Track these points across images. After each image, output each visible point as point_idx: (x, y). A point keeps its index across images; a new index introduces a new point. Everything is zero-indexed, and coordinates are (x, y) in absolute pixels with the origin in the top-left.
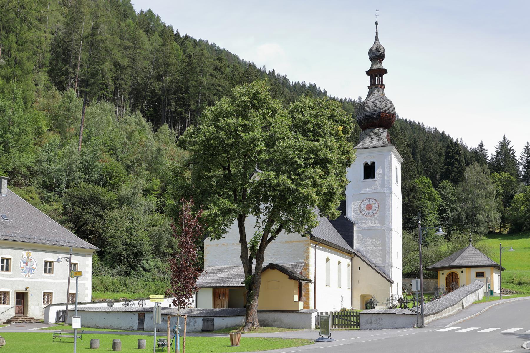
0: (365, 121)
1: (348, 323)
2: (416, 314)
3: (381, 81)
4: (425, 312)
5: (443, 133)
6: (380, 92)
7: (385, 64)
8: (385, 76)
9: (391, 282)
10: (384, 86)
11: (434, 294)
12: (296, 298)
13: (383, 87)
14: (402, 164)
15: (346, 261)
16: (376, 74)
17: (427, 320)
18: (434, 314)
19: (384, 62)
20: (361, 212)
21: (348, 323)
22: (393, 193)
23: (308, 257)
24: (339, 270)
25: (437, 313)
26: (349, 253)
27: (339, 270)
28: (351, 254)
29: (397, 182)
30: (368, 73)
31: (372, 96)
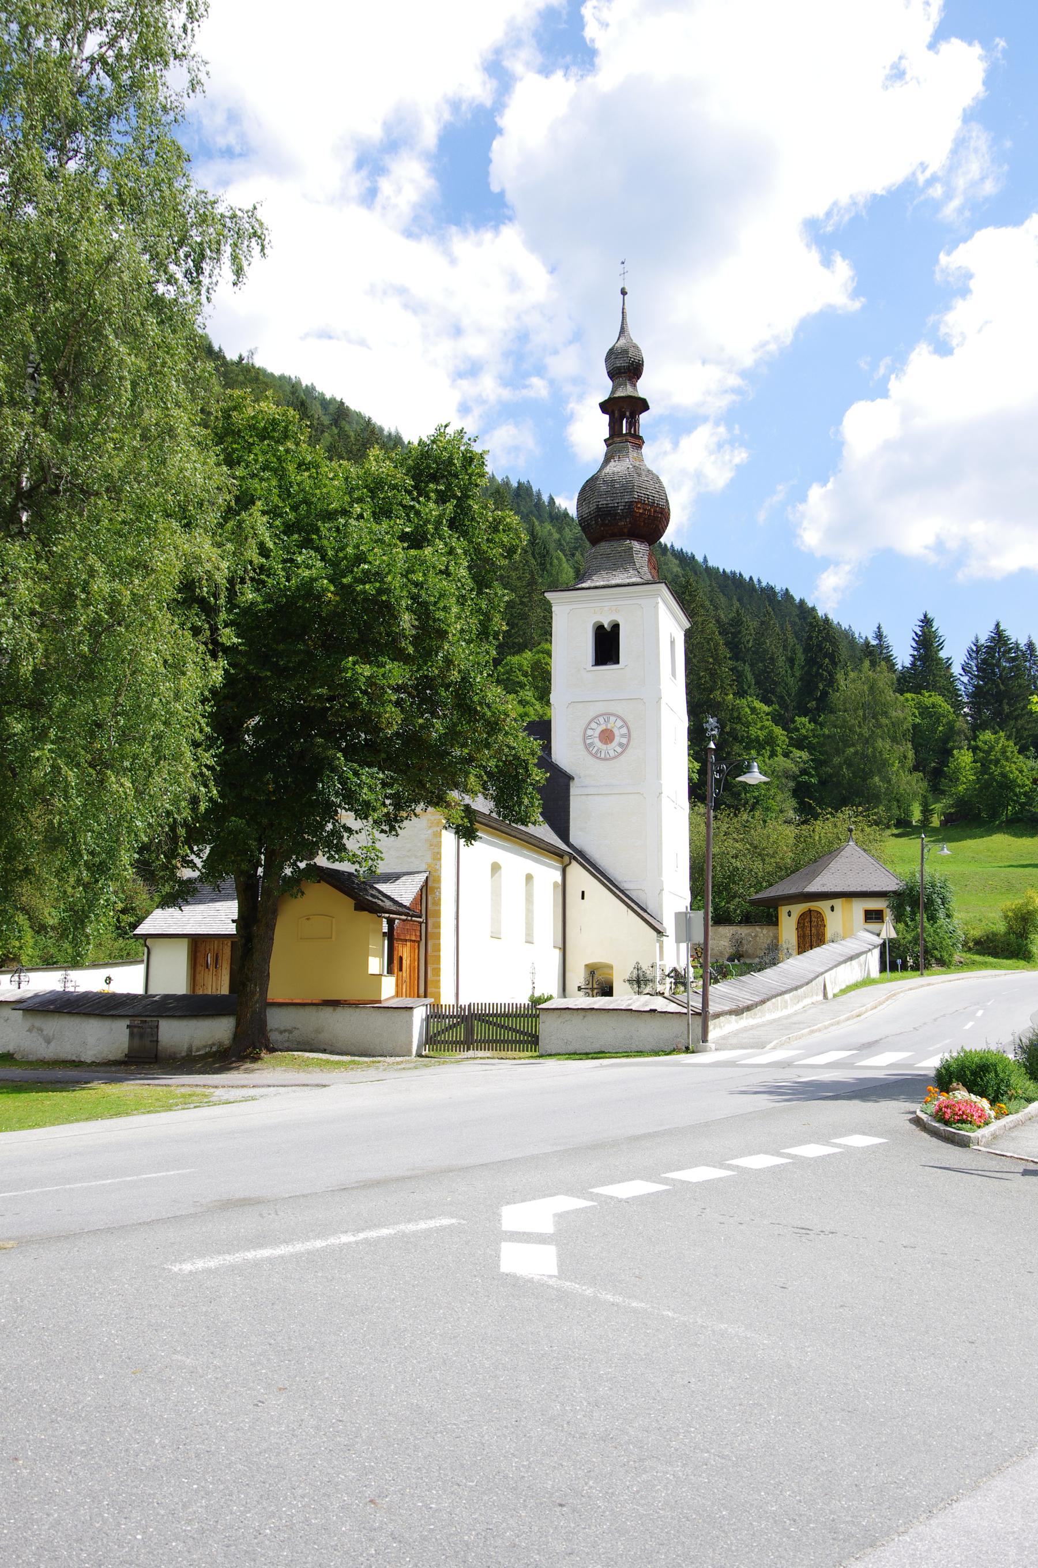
0: (596, 523)
1: (511, 1036)
2: (685, 1011)
3: (633, 423)
4: (712, 1008)
5: (500, 131)
6: (633, 453)
7: (644, 387)
8: (644, 418)
9: (659, 932)
10: (640, 438)
11: (742, 962)
12: (375, 965)
13: (638, 442)
14: (689, 635)
15: (547, 874)
16: (624, 413)
17: (716, 1031)
18: (738, 1012)
19: (640, 383)
20: (588, 747)
21: (511, 1036)
22: (663, 701)
23: (437, 856)
24: (496, 893)
25: (748, 1008)
26: (558, 854)
27: (496, 893)
28: (561, 856)
29: (674, 674)
30: (605, 407)
31: (612, 463)
